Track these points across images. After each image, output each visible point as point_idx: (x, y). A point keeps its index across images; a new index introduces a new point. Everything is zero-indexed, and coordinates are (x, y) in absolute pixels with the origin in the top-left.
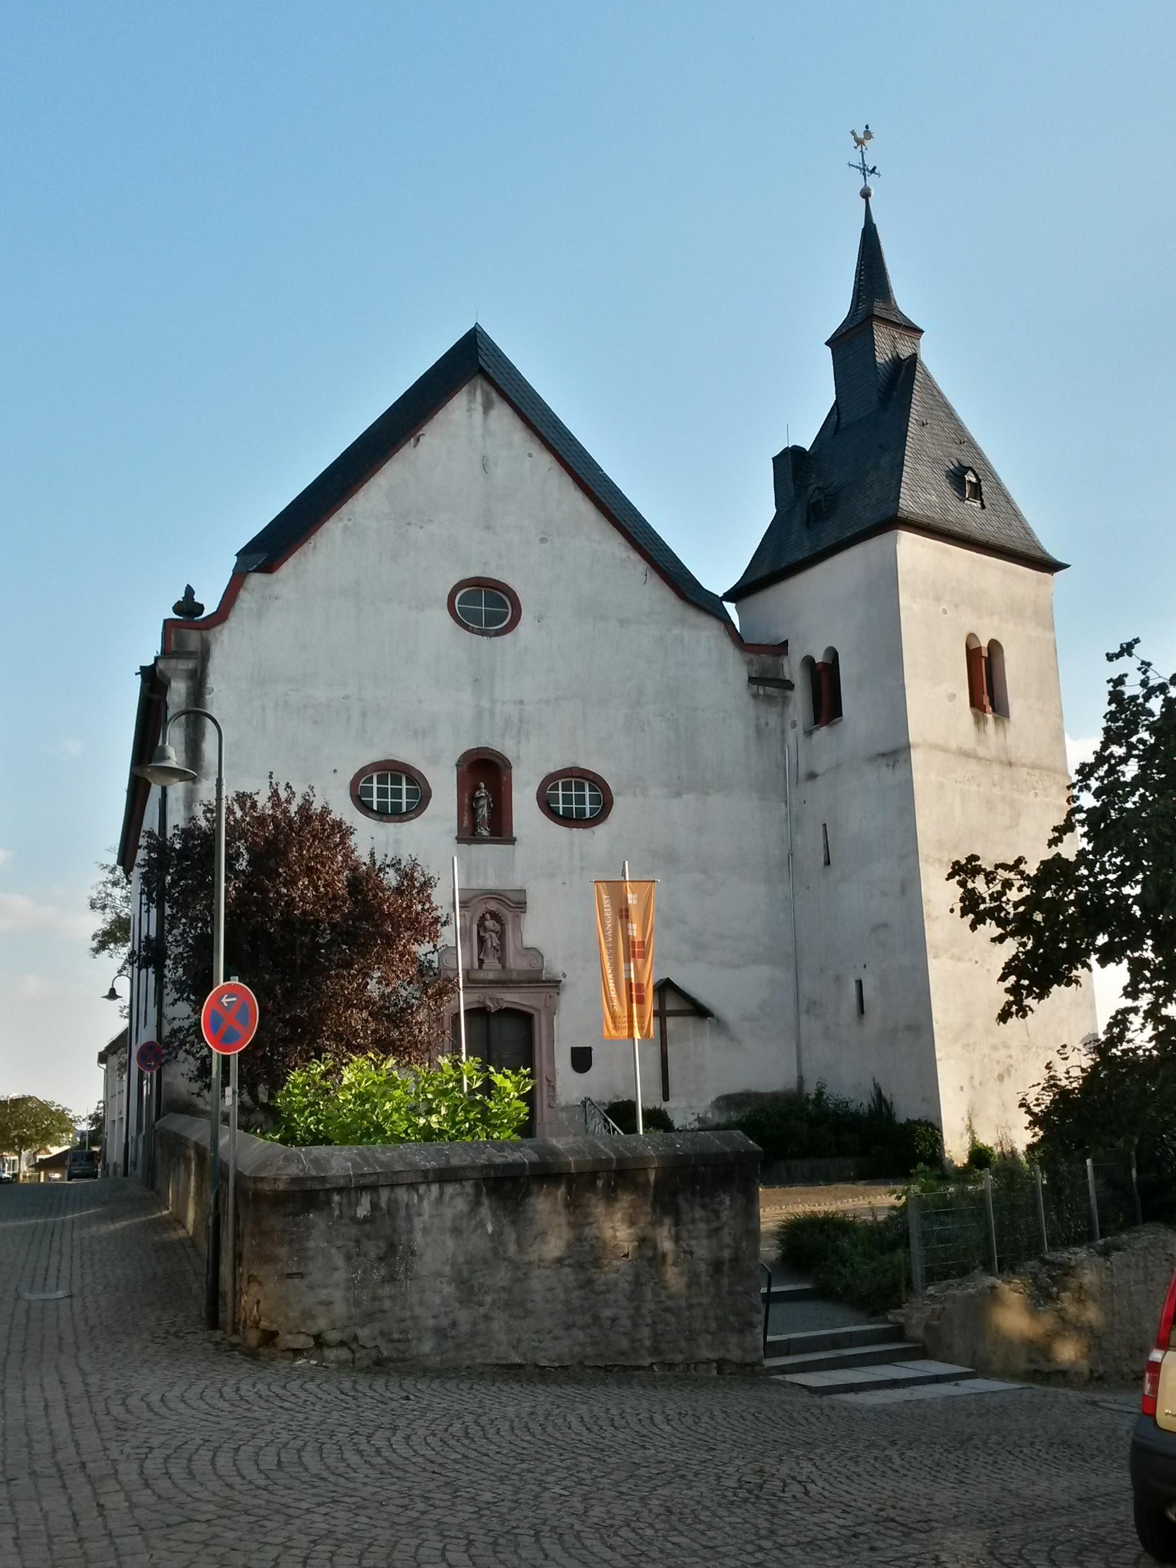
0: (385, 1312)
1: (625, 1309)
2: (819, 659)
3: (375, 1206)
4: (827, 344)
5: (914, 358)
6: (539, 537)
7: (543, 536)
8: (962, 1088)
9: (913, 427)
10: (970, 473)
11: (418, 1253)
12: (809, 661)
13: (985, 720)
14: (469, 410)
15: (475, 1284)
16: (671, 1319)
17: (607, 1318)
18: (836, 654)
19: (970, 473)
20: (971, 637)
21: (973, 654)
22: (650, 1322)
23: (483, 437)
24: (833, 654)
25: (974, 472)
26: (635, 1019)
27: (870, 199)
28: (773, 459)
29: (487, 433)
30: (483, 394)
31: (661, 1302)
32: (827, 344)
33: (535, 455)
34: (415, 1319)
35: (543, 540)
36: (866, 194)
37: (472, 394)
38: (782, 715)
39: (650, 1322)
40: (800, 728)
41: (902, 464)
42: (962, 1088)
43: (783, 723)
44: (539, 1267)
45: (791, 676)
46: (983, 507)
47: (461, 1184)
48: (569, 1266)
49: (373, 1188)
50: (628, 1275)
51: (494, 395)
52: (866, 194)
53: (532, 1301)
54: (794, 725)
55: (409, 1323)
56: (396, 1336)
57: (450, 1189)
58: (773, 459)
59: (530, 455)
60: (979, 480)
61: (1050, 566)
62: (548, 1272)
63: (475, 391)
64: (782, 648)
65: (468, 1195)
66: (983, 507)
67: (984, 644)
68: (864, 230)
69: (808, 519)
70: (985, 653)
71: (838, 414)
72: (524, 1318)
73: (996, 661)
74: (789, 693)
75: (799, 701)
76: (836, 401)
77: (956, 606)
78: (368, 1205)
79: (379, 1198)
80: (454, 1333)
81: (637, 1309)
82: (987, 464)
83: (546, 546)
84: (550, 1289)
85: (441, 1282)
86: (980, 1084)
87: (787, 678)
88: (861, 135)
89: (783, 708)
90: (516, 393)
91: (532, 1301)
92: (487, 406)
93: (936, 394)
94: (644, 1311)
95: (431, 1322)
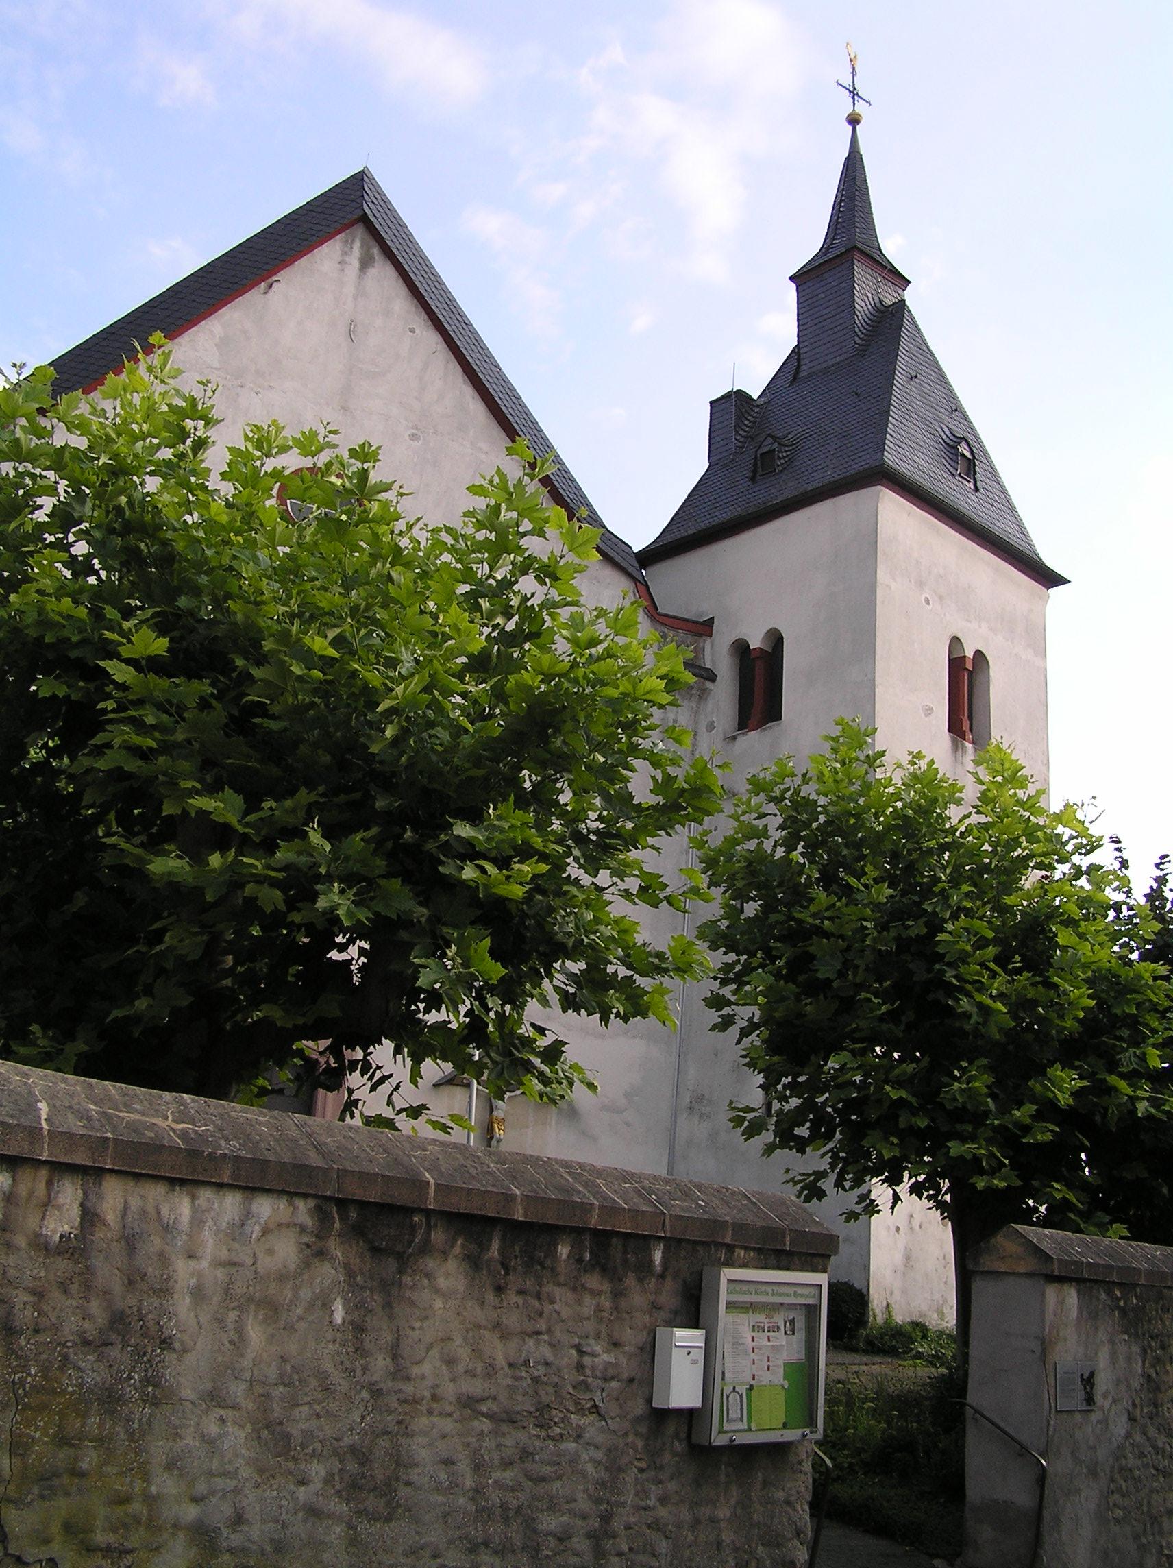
0: (82, 1475)
1: (584, 1517)
2: (755, 643)
3: (89, 1217)
4: (791, 278)
5: (901, 305)
6: (409, 432)
7: (414, 431)
8: (898, 1229)
9: (900, 378)
10: (963, 444)
11: (177, 1346)
12: (741, 648)
13: (964, 751)
14: (345, 253)
15: (294, 1432)
16: (663, 1546)
17: (550, 1533)
18: (781, 638)
19: (963, 444)
20: (955, 642)
21: (957, 665)
22: (625, 1548)
23: (355, 298)
24: (776, 639)
25: (969, 445)
26: (966, 705)
27: (858, 127)
28: (711, 403)
29: (360, 293)
30: (362, 247)
31: (646, 1509)
32: (791, 278)
33: (417, 331)
34: (151, 1500)
35: (414, 437)
36: (854, 120)
37: (349, 243)
38: (696, 713)
39: (625, 1548)
40: (718, 734)
41: (887, 413)
42: (898, 1229)
43: (696, 722)
44: (430, 1412)
45: (714, 663)
46: (977, 490)
47: (291, 1203)
48: (490, 1416)
49: (90, 1173)
50: (597, 1447)
51: (376, 251)
52: (854, 120)
53: (408, 1483)
54: (711, 727)
55: (136, 1507)
56: (101, 1538)
57: (265, 1208)
58: (711, 403)
59: (412, 331)
60: (974, 458)
61: (1050, 579)
62: (448, 1425)
63: (353, 242)
64: (704, 628)
65: (303, 1229)
66: (977, 490)
67: (970, 654)
68: (847, 159)
69: (755, 472)
70: (969, 666)
71: (799, 360)
72: (388, 1519)
73: (979, 679)
74: (708, 684)
75: (724, 693)
76: (796, 352)
77: (941, 598)
78: (75, 1212)
79: (100, 1197)
80: (236, 1539)
81: (606, 1518)
82: (980, 443)
83: (415, 444)
84: (448, 1462)
85: (222, 1420)
86: (920, 1227)
87: (708, 666)
88: (852, 57)
89: (699, 703)
90: (404, 254)
91: (408, 1483)
92: (366, 263)
93: (925, 349)
94: (617, 1524)
95: (191, 1512)
